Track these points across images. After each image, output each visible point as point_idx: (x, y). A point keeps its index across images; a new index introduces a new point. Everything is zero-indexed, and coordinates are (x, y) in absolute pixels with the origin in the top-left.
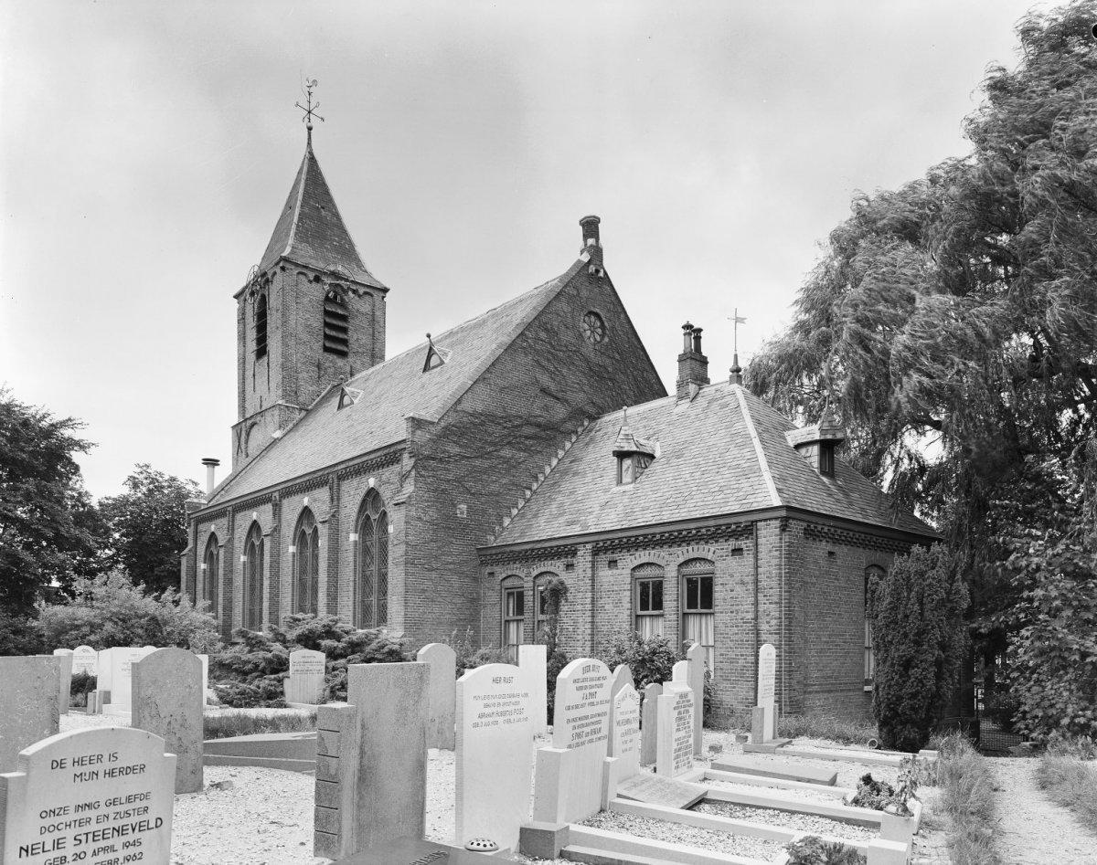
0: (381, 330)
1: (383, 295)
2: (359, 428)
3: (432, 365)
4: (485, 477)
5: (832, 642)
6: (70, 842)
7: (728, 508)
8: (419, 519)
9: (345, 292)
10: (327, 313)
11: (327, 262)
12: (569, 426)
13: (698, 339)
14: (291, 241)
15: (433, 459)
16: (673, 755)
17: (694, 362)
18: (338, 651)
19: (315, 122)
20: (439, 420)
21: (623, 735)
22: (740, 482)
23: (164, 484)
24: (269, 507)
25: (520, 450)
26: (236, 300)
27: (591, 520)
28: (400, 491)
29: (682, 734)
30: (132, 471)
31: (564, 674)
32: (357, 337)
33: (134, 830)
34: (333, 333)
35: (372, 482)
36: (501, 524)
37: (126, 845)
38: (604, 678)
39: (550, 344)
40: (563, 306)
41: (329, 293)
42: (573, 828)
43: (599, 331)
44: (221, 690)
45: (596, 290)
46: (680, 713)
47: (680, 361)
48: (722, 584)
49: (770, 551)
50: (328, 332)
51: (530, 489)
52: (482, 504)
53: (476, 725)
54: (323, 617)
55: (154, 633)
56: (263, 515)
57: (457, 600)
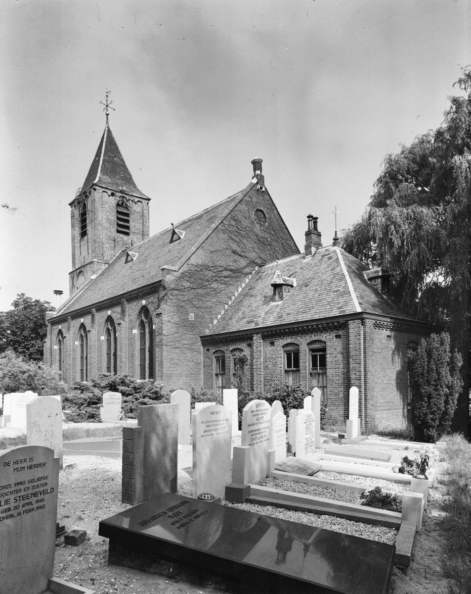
0: (147, 220)
1: (147, 201)
2: (137, 273)
3: (174, 240)
4: (203, 299)
5: (390, 383)
6: (12, 501)
7: (332, 314)
8: (169, 321)
9: (127, 201)
10: (118, 212)
11: (117, 185)
12: (247, 270)
13: (315, 223)
14: (99, 175)
15: (176, 290)
16: (304, 447)
17: (313, 233)
18: (127, 392)
19: (110, 111)
20: (179, 269)
21: (278, 437)
22: (339, 299)
23: (33, 304)
25: (222, 284)
26: (70, 206)
27: (260, 320)
28: (159, 307)
29: (308, 436)
30: (15, 298)
31: (246, 409)
32: (134, 224)
33: (41, 494)
34: (122, 223)
35: (144, 302)
36: (212, 323)
37: (37, 501)
38: (267, 409)
39: (237, 227)
40: (243, 207)
41: (119, 201)
42: (253, 486)
43: (263, 219)
44: (68, 414)
45: (261, 198)
46: (307, 425)
47: (306, 235)
48: (330, 354)
49: (356, 336)
50: (119, 222)
51: (228, 304)
52: (202, 313)
53: (202, 436)
54: (121, 374)
55: (31, 384)
57: (190, 364)
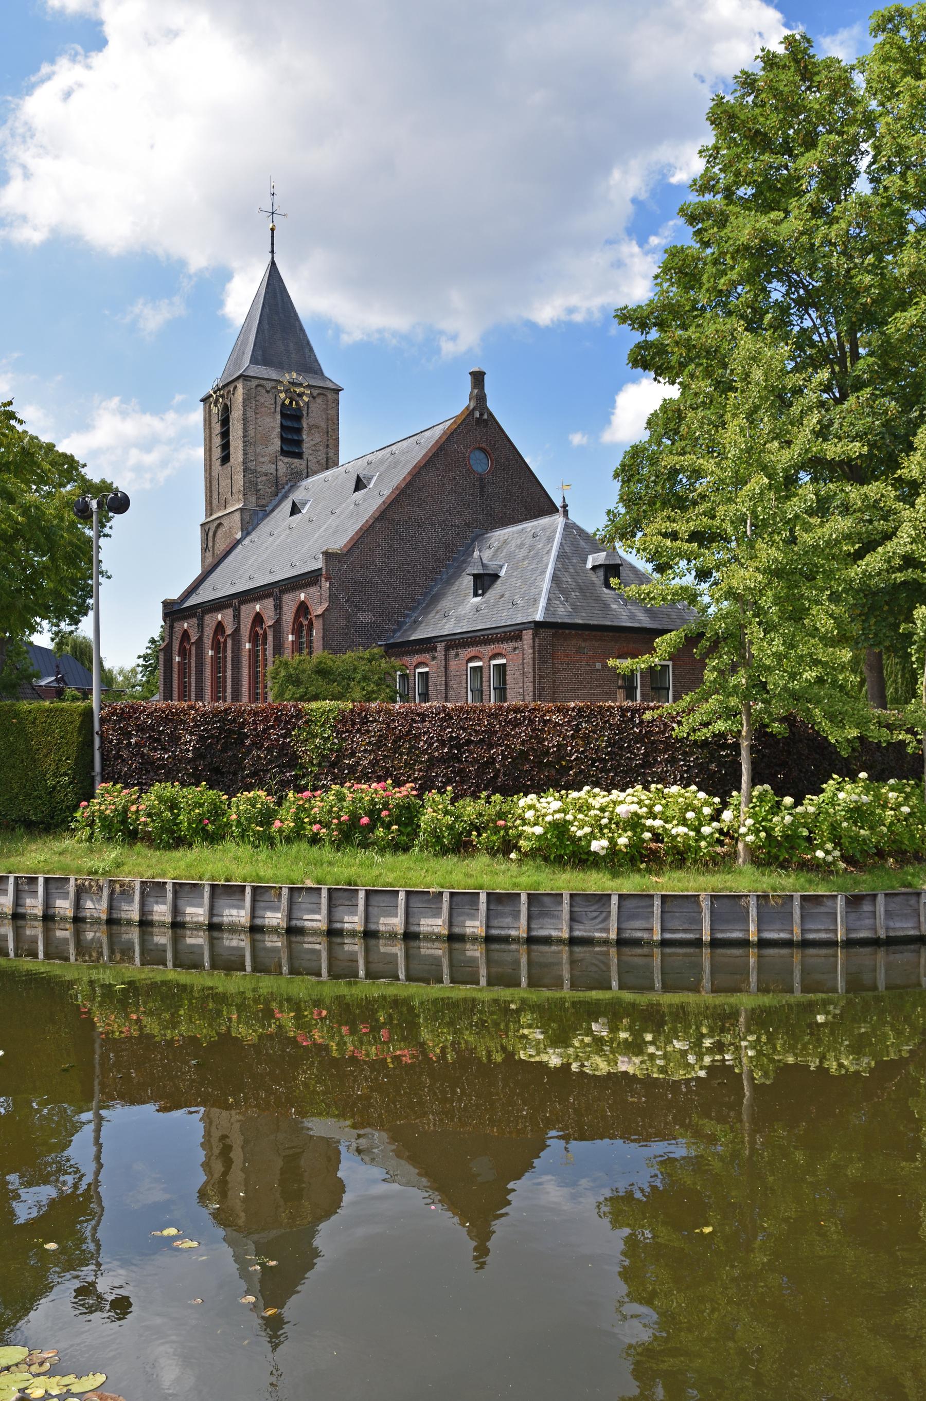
24: (229, 612)
56: (224, 616)
